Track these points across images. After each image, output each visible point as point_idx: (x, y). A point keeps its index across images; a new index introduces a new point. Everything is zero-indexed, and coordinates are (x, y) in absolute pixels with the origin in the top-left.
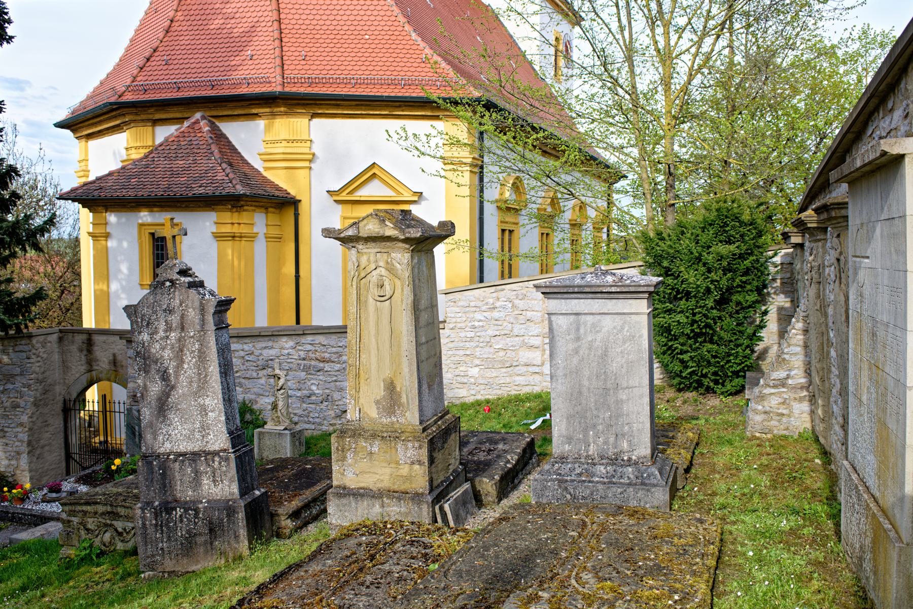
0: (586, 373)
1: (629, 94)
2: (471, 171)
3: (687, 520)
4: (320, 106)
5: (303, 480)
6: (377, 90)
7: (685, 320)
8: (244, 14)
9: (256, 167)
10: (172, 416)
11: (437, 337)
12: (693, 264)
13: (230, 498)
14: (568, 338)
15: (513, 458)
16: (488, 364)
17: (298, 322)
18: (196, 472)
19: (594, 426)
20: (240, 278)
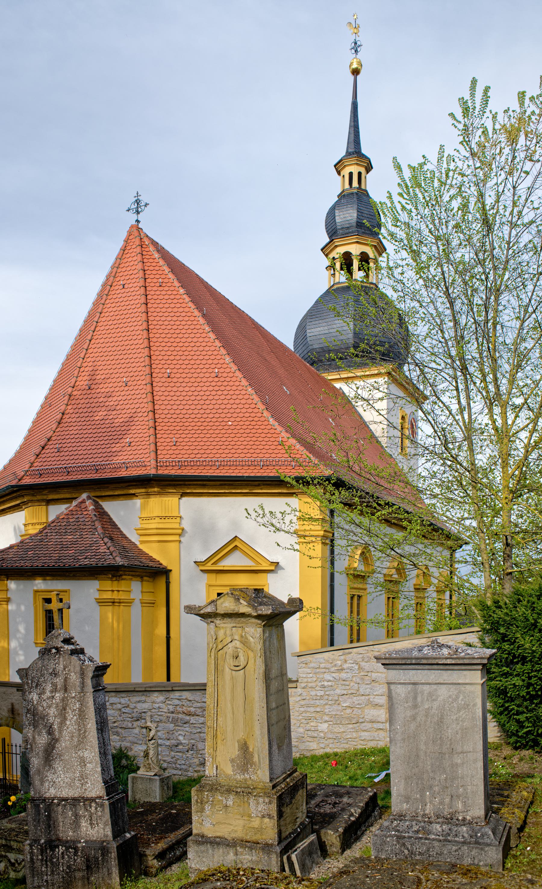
0: (423, 738)
1: (468, 471)
2: (323, 543)
3: (518, 881)
4: (188, 486)
5: (169, 824)
6: (238, 471)
7: (521, 683)
8: (124, 406)
9: (133, 540)
10: (56, 766)
11: (286, 702)
12: (529, 630)
13: (104, 839)
14: (406, 705)
15: (356, 812)
16: (337, 720)
17: (168, 679)
18: (76, 815)
19: (431, 787)
20: (118, 638)
